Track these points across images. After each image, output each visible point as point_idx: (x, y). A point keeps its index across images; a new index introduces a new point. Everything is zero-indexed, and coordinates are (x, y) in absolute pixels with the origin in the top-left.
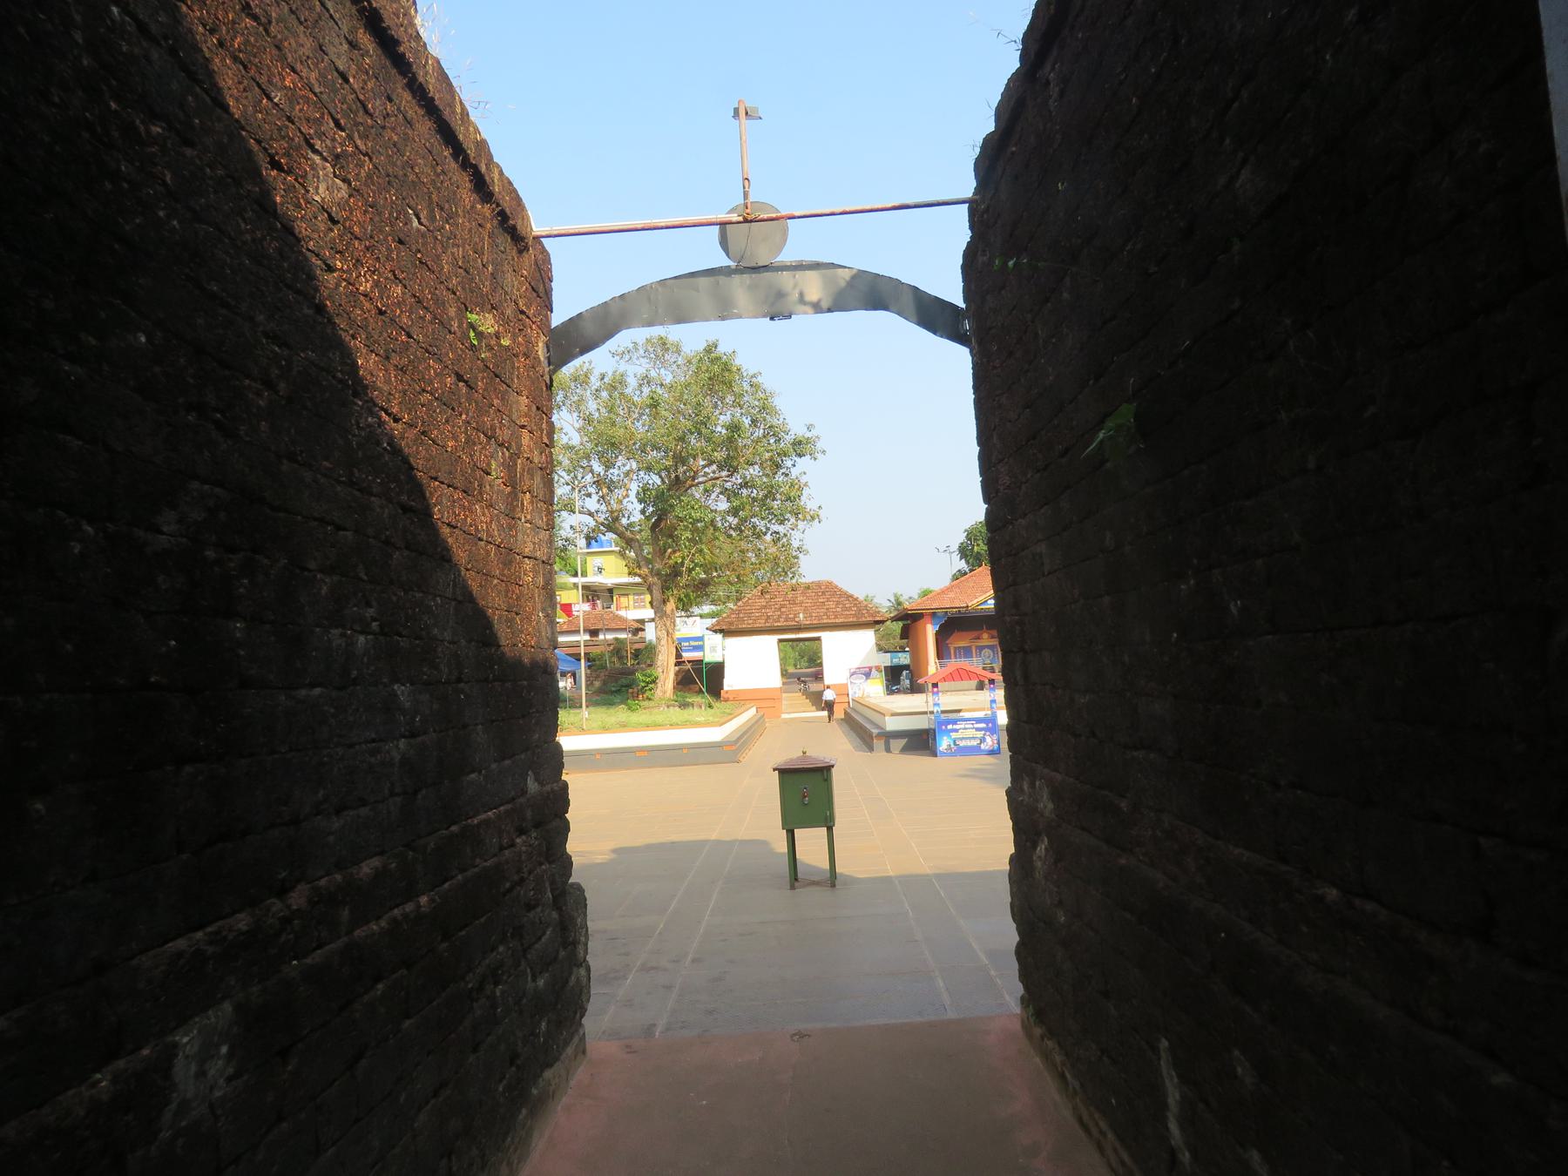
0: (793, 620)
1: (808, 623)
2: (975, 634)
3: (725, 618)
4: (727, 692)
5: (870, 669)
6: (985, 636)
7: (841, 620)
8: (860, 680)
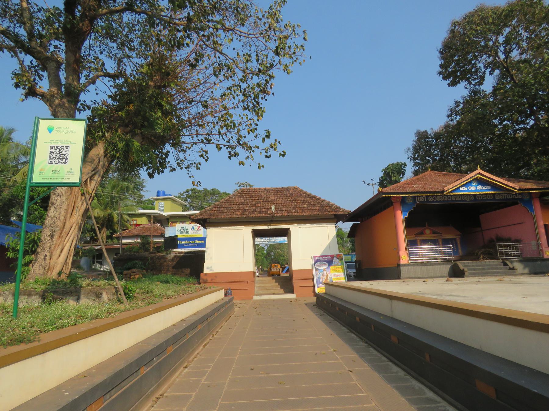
1: (279, 215)
3: (208, 210)
4: (206, 274)
5: (332, 257)
6: (428, 231)
7: (307, 214)
8: (323, 267)
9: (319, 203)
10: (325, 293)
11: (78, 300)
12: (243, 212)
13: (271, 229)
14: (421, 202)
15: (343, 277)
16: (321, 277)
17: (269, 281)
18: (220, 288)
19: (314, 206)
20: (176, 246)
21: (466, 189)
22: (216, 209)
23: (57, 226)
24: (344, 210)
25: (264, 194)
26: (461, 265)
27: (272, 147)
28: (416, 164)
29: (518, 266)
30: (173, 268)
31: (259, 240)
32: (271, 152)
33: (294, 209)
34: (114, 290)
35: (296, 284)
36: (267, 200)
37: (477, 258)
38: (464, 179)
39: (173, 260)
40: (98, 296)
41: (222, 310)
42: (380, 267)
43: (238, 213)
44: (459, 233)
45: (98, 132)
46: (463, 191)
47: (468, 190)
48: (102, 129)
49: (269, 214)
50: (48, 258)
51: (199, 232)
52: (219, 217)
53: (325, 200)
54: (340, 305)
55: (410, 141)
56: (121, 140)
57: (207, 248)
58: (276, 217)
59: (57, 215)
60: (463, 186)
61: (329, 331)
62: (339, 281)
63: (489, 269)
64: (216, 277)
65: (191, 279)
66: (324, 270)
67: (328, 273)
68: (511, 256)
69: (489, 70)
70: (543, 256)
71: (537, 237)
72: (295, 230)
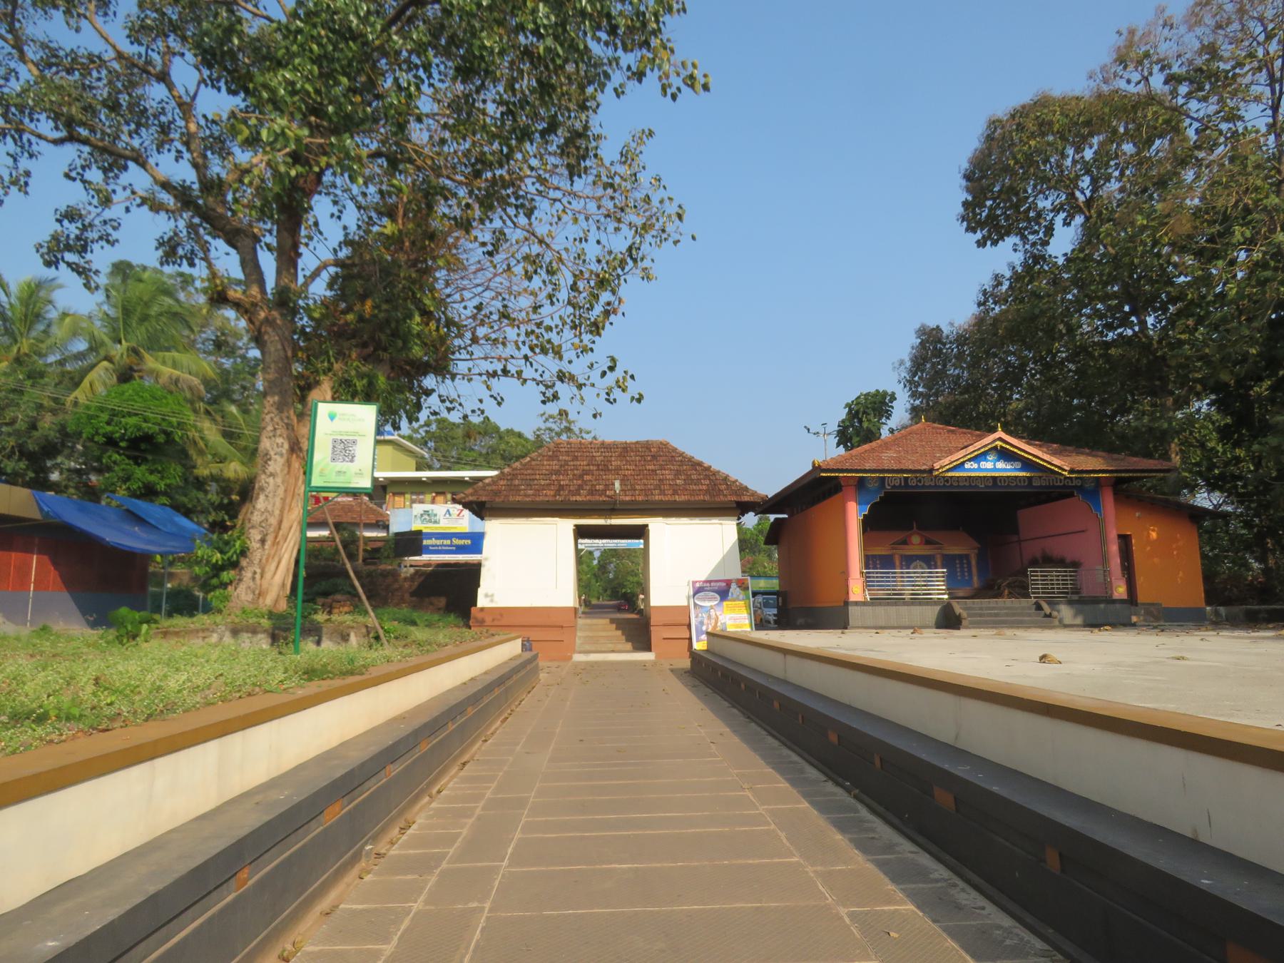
0: (603, 492)
1: (628, 498)
2: (899, 536)
4: (482, 609)
5: (728, 583)
6: (916, 539)
7: (683, 498)
9: (707, 477)
10: (707, 651)
11: (318, 643)
12: (559, 490)
13: (611, 526)
14: (894, 487)
15: (747, 622)
16: (706, 621)
17: (602, 626)
18: (513, 635)
19: (698, 482)
20: (419, 550)
21: (975, 466)
22: (505, 482)
23: (270, 525)
24: (754, 494)
25: (599, 454)
26: (958, 608)
27: (620, 387)
28: (914, 395)
29: (1066, 612)
30: (413, 594)
31: (585, 543)
32: (617, 393)
33: (658, 487)
34: (364, 630)
35: (656, 634)
36: (605, 468)
37: (999, 595)
38: (978, 445)
39: (413, 578)
40: (345, 638)
41: (523, 673)
42: (817, 605)
43: (549, 493)
44: (977, 545)
45: (323, 362)
46: (969, 470)
47: (979, 469)
48: (329, 356)
49: (608, 496)
50: (258, 576)
51: (461, 521)
52: (511, 499)
53: (719, 472)
54: (723, 667)
55: (905, 345)
56: (361, 376)
57: (486, 559)
58: (623, 503)
59: (270, 508)
60: (969, 460)
61: (700, 705)
62: (739, 630)
63: (1007, 615)
64: (501, 615)
65: (452, 618)
66: (712, 607)
67: (718, 613)
68: (1054, 593)
69: (1062, 215)
70: (1112, 593)
71: (1104, 559)
72: (658, 527)
